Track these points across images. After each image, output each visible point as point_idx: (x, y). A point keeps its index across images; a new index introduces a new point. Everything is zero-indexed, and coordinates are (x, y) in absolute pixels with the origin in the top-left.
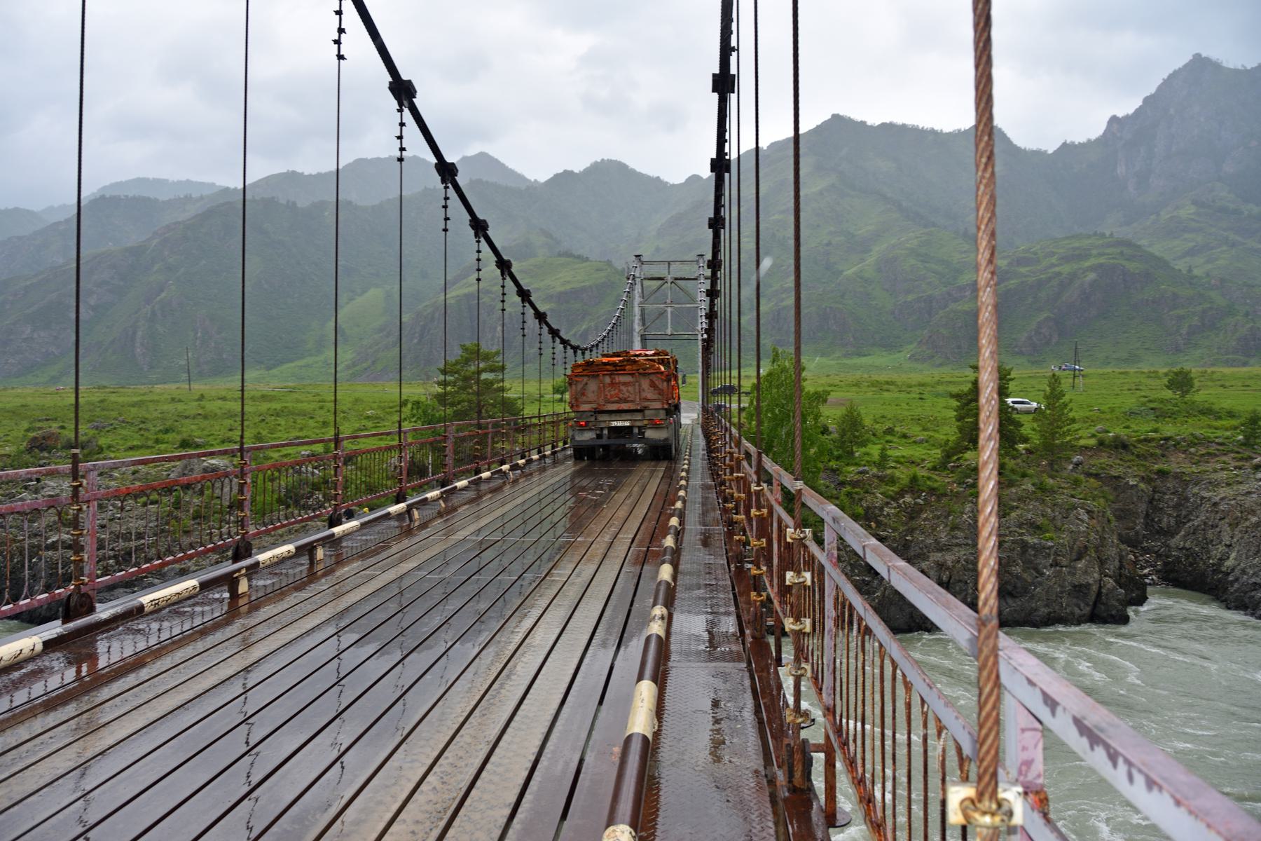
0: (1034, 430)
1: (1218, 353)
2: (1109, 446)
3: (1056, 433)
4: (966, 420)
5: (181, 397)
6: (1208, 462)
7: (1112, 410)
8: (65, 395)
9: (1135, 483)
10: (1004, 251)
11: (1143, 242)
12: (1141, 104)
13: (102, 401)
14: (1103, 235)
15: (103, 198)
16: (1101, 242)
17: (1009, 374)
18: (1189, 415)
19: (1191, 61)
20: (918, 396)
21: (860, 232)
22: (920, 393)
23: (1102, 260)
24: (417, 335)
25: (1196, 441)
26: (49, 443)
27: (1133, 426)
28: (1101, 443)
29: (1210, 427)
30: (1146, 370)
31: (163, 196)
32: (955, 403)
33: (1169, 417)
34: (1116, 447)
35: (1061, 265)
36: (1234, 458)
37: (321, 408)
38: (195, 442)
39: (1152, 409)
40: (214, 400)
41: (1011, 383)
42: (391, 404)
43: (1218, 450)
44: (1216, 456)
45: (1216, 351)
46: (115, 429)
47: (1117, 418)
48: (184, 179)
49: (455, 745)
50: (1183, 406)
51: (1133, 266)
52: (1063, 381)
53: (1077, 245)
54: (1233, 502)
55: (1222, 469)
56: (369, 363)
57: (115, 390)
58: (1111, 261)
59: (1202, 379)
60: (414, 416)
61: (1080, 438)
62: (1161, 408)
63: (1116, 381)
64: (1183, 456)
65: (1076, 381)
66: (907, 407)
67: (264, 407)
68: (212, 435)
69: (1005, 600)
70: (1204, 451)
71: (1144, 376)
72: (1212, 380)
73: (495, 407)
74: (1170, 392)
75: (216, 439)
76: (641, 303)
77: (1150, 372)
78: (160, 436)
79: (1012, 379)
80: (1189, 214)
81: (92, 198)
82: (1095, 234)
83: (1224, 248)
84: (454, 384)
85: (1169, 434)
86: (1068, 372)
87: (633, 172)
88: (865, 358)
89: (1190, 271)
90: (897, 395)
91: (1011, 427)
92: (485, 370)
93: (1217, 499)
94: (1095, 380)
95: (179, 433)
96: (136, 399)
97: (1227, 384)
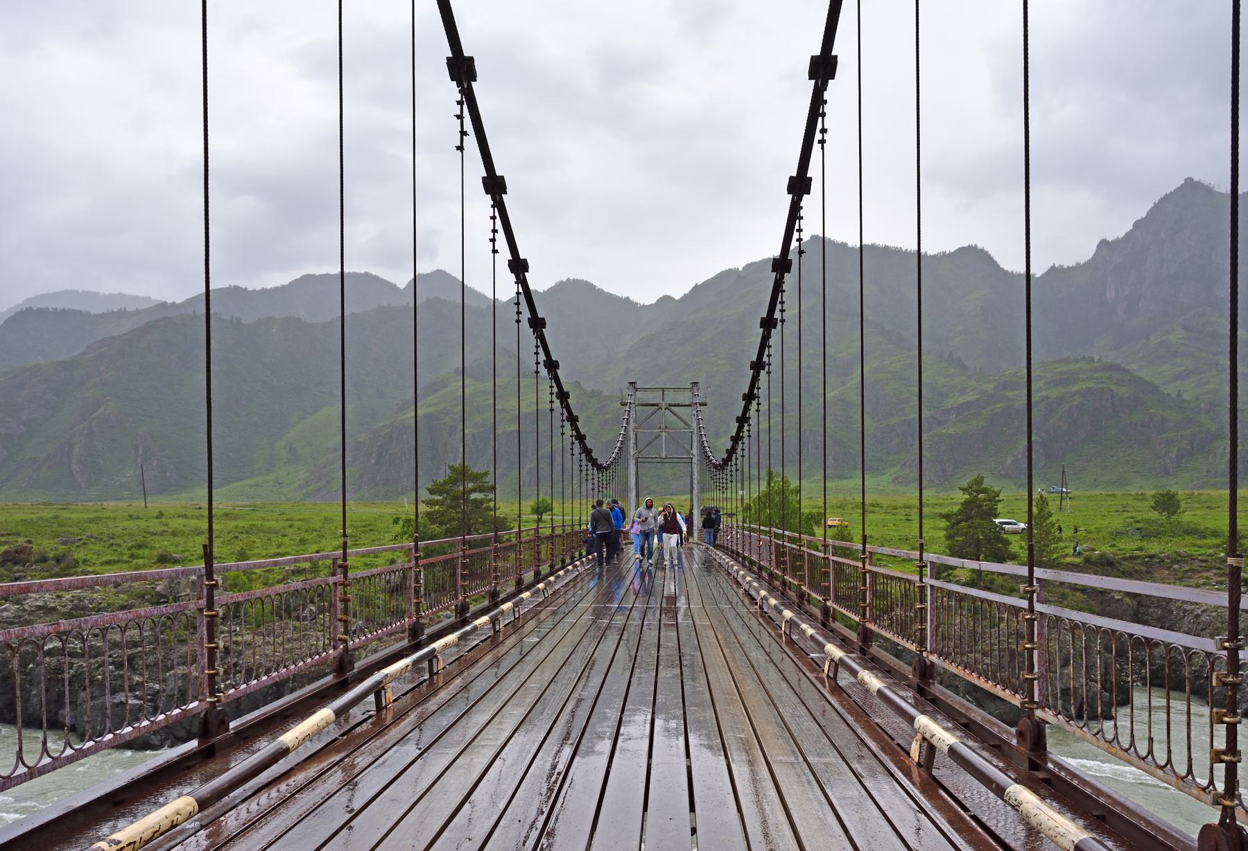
0: (1022, 548)
1: (1207, 476)
2: (1095, 564)
3: (1044, 550)
4: (956, 538)
5: (137, 514)
6: (1191, 578)
7: (1099, 530)
8: (13, 511)
9: (1120, 597)
10: (990, 376)
11: (1133, 367)
12: (1131, 228)
13: (56, 517)
14: (1091, 360)
15: (29, 309)
16: (1089, 366)
17: (998, 496)
18: (1174, 535)
19: (1182, 185)
20: (904, 518)
21: (840, 355)
22: (907, 515)
23: (1090, 384)
24: (374, 455)
25: (1179, 558)
26: (22, 556)
27: (1119, 544)
28: (1088, 560)
29: (1194, 545)
30: (1133, 493)
31: (95, 310)
32: (944, 523)
33: (1155, 537)
34: (1102, 565)
35: (1048, 389)
36: (1215, 574)
37: (291, 526)
38: (173, 558)
39: (1138, 529)
40: (174, 517)
41: (1000, 505)
42: (364, 524)
43: (1200, 566)
44: (1199, 572)
45: (1205, 474)
46: (85, 544)
47: (1103, 537)
48: (116, 292)
49: (913, 460)
50: (1169, 526)
51: (1124, 391)
52: (1050, 504)
53: (1064, 369)
54: (1214, 614)
55: (1204, 584)
56: (324, 482)
57: (65, 507)
58: (1100, 386)
59: (1189, 501)
60: (406, 533)
61: (1067, 555)
62: (1147, 529)
63: (1104, 503)
64: (1167, 572)
65: (1063, 503)
66: (894, 528)
67: (231, 524)
68: (187, 551)
69: (995, 702)
70: (1187, 568)
71: (1131, 498)
72: (1199, 502)
73: (484, 525)
74: (1156, 513)
75: (193, 555)
76: (636, 428)
77: (1137, 494)
78: (135, 551)
79: (1000, 501)
80: (1180, 339)
81: (18, 310)
82: (1084, 358)
83: (1214, 372)
84: (441, 503)
85: (1153, 552)
86: (1055, 494)
87: (601, 292)
88: (845, 481)
89: (1179, 394)
90: (883, 516)
91: (1000, 545)
92: (474, 490)
93: (1199, 611)
94: (1082, 503)
95: (153, 548)
96: (91, 516)
97: (1213, 506)
